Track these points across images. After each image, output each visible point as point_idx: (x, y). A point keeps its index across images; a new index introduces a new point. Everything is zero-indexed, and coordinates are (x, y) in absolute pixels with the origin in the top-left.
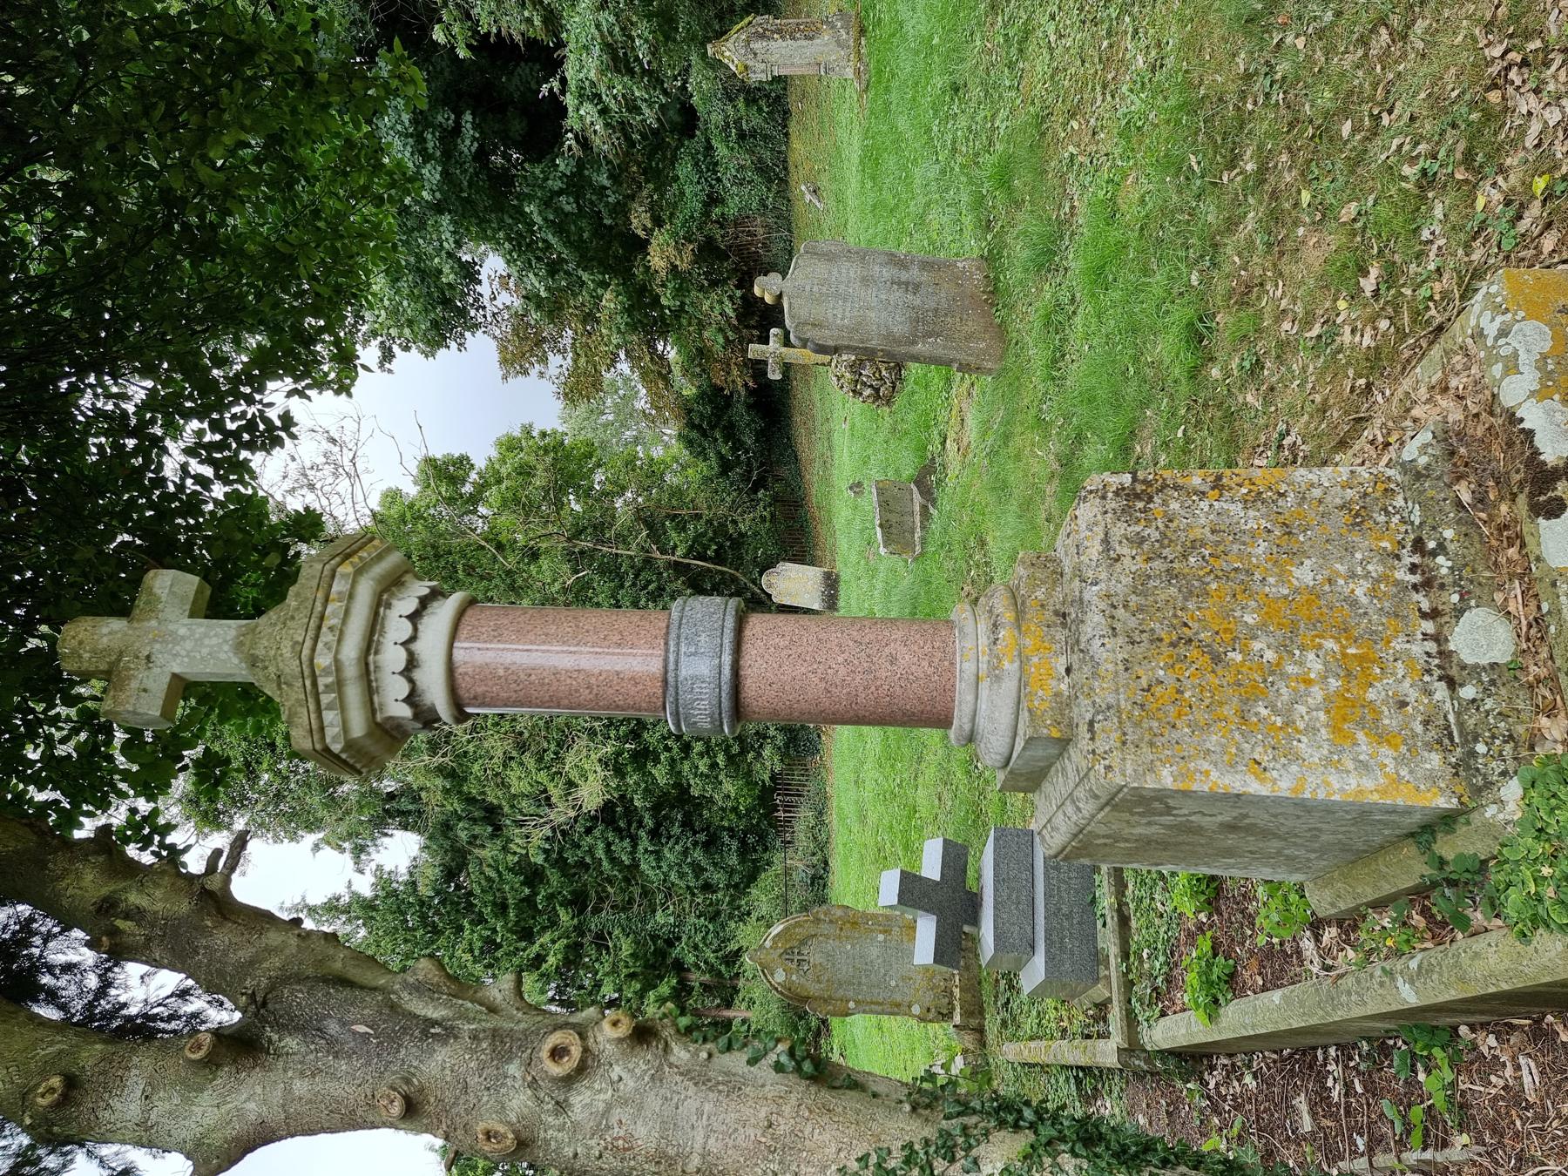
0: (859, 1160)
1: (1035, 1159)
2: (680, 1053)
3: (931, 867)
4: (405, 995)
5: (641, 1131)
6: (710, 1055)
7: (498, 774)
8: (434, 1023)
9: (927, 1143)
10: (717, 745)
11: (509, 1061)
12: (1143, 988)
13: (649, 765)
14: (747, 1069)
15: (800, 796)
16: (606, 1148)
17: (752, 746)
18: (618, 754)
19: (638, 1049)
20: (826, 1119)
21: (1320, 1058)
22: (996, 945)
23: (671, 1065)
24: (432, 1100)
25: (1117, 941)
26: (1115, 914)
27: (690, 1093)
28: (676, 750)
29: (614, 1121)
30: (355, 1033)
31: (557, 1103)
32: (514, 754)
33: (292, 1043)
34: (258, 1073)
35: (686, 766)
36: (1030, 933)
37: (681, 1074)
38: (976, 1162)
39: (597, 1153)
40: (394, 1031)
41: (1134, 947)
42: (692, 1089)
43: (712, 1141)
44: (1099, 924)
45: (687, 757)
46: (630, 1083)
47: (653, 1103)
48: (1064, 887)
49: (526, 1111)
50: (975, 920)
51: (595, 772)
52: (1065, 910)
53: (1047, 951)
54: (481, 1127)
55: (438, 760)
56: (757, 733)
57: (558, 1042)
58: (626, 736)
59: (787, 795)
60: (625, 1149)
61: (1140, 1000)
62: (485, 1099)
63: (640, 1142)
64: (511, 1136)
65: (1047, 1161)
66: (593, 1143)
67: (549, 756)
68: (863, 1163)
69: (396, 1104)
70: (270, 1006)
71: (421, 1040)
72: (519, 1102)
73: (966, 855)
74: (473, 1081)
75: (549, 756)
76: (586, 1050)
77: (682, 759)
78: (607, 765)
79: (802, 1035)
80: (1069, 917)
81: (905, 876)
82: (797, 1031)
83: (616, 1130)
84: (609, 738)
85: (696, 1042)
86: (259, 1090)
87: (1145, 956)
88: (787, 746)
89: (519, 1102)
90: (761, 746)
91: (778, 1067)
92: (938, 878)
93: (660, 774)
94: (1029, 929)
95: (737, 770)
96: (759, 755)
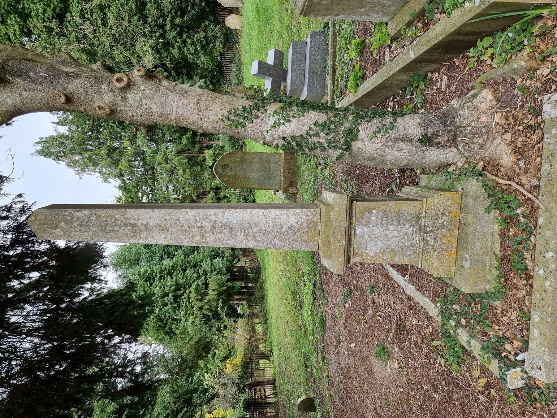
0: (228, 112)
1: (285, 108)
2: (165, 83)
3: (270, 60)
4: (58, 65)
5: (154, 106)
6: (176, 84)
7: (109, 53)
8: (71, 73)
9: (250, 106)
10: (197, 41)
11: (102, 84)
12: (338, 92)
13: (171, 50)
14: (189, 88)
15: (231, 62)
16: (143, 113)
17: (211, 41)
18: (157, 44)
19: (149, 80)
20: (217, 100)
21: (388, 102)
22: (291, 85)
23: (162, 86)
24: (76, 97)
25: (331, 78)
26: (332, 69)
27: (169, 95)
28: (180, 43)
29: (144, 103)
30: (41, 76)
31: (122, 97)
32: (114, 44)
33: (18, 80)
34: (7, 89)
35: (185, 50)
36: (303, 80)
37: (166, 89)
38: (266, 110)
39: (140, 114)
40: (56, 75)
41: (336, 78)
42: (170, 94)
43: (179, 109)
44: (327, 74)
45: (185, 46)
46: (147, 92)
47: (157, 98)
48: (316, 62)
49: (111, 100)
50: (285, 80)
51: (149, 52)
52: (316, 70)
53: (308, 86)
54: (96, 105)
55: (82, 46)
56: (213, 35)
57: (118, 77)
58: (159, 36)
59: (226, 62)
60: (149, 113)
61: (336, 96)
62: (95, 96)
63: (154, 110)
64: (107, 108)
65: (288, 109)
66: (138, 111)
67: (128, 45)
68: (229, 113)
69: (62, 97)
70: (6, 68)
71: (66, 77)
72: (108, 97)
73: (283, 56)
74: (90, 91)
75: (128, 45)
76: (129, 79)
77: (183, 47)
78: (153, 49)
79: (236, 147)
80: (316, 73)
81: (260, 62)
82: (235, 146)
83: (145, 106)
84: (152, 37)
85: (171, 81)
86: (9, 94)
87: (339, 81)
88: (225, 41)
89: (108, 97)
90: (215, 41)
91: (200, 87)
92: (272, 64)
93: (175, 52)
94: (303, 78)
95: (206, 51)
96: (214, 45)
